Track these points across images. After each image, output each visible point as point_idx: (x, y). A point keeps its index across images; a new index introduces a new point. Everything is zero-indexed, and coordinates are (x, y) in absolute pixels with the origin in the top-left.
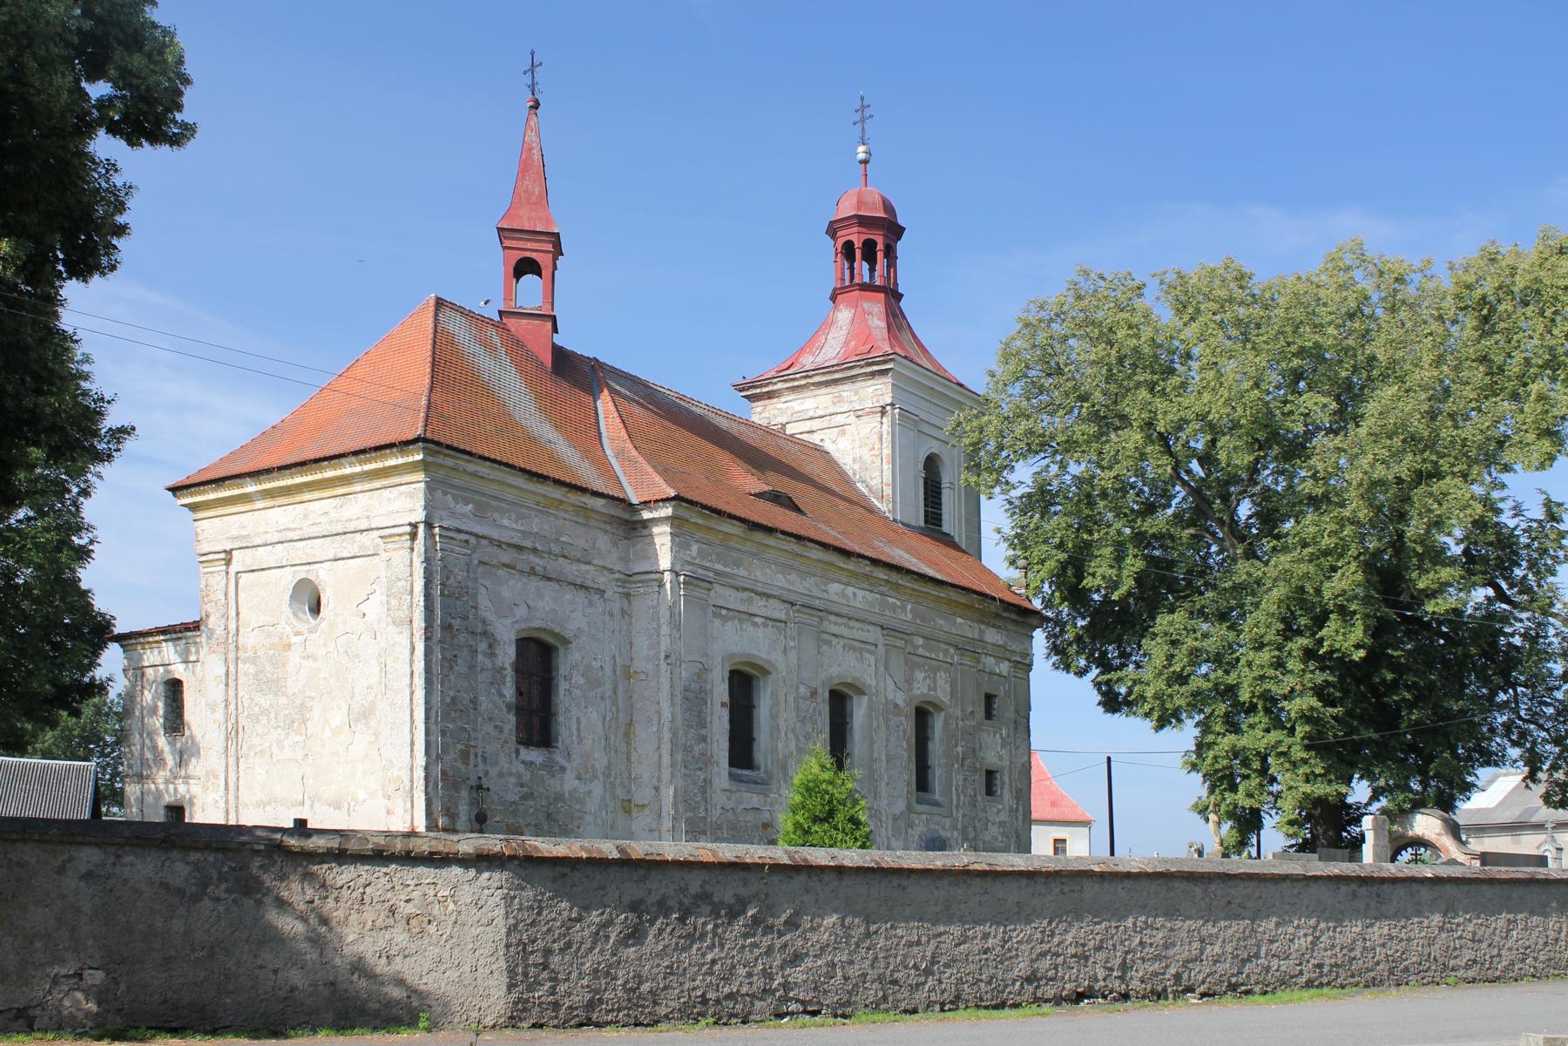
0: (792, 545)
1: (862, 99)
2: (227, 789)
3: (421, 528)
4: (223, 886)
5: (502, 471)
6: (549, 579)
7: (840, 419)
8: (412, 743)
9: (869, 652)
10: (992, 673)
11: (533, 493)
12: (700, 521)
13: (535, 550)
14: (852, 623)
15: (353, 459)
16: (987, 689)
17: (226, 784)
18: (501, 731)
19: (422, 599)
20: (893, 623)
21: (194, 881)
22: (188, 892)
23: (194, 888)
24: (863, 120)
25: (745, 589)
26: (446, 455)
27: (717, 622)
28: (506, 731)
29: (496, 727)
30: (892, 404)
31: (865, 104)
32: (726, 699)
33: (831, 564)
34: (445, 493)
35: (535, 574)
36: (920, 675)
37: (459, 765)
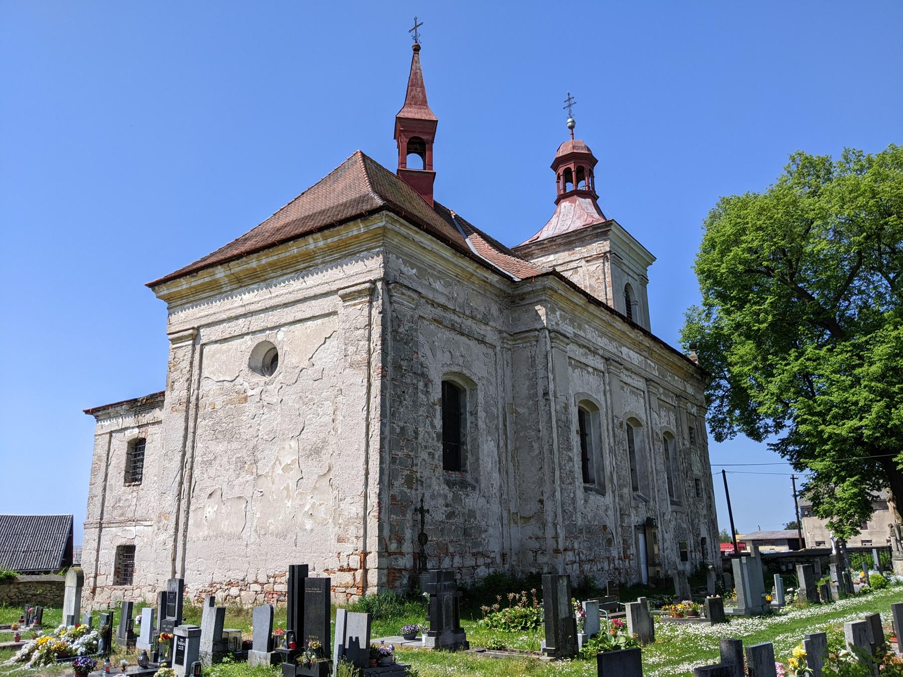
0: (607, 317)
1: (569, 94)
2: (177, 529)
3: (379, 285)
5: (438, 244)
6: (463, 334)
7: (574, 265)
12: (563, 293)
14: (633, 376)
15: (319, 235)
17: (177, 524)
19: (379, 343)
20: (651, 377)
25: (584, 347)
26: (402, 224)
27: (570, 369)
28: (437, 456)
29: (430, 454)
30: (610, 252)
31: (571, 96)
33: (624, 333)
34: (398, 258)
35: (455, 330)
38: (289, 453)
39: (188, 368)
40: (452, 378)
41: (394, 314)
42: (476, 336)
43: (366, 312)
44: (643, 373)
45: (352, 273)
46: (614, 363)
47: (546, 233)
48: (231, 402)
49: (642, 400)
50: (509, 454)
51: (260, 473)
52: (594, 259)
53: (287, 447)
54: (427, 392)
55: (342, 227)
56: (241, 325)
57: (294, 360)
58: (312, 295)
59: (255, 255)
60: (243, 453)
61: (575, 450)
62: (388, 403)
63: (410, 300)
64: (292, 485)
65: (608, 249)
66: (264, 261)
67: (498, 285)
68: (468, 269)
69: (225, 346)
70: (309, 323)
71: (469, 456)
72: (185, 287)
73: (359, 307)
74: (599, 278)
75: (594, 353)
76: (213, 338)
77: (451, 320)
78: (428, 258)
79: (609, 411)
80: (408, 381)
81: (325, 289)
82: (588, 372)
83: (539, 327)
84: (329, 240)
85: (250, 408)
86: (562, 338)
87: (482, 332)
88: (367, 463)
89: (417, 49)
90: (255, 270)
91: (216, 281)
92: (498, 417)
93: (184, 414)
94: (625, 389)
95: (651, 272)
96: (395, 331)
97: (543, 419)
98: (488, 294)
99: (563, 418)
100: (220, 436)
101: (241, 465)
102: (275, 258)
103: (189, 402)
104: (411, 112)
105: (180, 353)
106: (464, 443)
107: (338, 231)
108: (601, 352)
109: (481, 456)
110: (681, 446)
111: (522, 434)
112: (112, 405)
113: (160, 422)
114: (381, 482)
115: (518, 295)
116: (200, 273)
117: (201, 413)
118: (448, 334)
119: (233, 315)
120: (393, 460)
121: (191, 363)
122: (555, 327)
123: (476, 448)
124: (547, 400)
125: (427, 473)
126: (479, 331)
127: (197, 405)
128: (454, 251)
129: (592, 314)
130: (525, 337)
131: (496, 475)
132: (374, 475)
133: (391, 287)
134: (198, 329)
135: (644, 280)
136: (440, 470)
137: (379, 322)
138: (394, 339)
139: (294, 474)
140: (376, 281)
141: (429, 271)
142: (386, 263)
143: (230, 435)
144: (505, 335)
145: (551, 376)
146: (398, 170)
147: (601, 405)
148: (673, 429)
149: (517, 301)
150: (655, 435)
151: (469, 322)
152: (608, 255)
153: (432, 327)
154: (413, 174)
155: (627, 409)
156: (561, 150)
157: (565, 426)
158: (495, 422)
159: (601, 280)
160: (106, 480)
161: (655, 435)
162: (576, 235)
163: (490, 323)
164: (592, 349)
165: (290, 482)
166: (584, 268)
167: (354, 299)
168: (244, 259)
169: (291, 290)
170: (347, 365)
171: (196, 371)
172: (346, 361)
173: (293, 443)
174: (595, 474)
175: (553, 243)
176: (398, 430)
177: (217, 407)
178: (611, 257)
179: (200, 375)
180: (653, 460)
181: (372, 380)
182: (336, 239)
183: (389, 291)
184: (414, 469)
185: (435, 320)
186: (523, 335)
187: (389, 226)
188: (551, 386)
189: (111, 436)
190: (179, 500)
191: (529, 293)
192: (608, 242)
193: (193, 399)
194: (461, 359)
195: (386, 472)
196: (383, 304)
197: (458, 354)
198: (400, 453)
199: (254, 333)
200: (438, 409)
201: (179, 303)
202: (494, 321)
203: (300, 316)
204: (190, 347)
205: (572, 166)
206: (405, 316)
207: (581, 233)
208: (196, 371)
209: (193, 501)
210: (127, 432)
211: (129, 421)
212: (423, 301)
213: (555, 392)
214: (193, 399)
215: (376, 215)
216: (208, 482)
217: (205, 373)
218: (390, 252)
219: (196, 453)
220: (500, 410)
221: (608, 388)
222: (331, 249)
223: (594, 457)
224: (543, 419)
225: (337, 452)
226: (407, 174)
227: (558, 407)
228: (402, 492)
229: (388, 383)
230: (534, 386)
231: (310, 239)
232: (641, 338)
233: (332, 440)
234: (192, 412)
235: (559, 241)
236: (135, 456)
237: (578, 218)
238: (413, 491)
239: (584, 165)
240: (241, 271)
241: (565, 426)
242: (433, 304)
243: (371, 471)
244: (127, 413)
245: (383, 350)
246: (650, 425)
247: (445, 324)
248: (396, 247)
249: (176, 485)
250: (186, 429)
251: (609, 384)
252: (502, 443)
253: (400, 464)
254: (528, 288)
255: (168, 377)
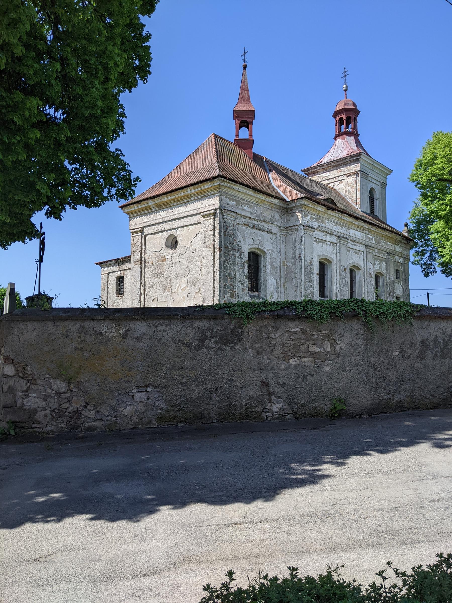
1: (345, 69)
3: (218, 211)
4: (214, 340)
5: (245, 189)
6: (259, 230)
7: (340, 178)
8: (214, 292)
9: (361, 254)
10: (398, 262)
11: (255, 197)
12: (311, 206)
13: (255, 219)
14: (357, 244)
15: (192, 187)
16: (396, 268)
18: (244, 286)
19: (218, 237)
20: (369, 244)
21: (197, 338)
22: (194, 345)
23: (197, 342)
24: (345, 76)
25: (325, 232)
26: (227, 182)
27: (315, 243)
28: (245, 285)
29: (242, 284)
30: (360, 170)
31: (346, 70)
32: (318, 272)
33: (351, 222)
34: (226, 197)
35: (255, 228)
36: (376, 263)
37: (230, 298)
38: (184, 283)
39: (140, 246)
40: (254, 250)
41: (225, 224)
42: (266, 230)
43: (212, 223)
44: (363, 242)
45: (206, 205)
46: (342, 239)
47: (326, 160)
48: (159, 261)
49: (362, 257)
50: (282, 284)
51: (172, 291)
52: (351, 175)
53: (183, 280)
54: (241, 257)
55: (202, 184)
56: (160, 227)
57: (184, 244)
58: (190, 214)
59: (166, 195)
60: (165, 283)
61: (315, 282)
62: (222, 263)
63: (232, 217)
64: (186, 296)
65: (359, 169)
66: (170, 198)
67: (278, 204)
68: (262, 198)
69: (155, 236)
70: (190, 227)
71: (262, 285)
72: (136, 208)
73: (210, 221)
74: (353, 186)
75: (331, 234)
76: (150, 232)
77: (253, 224)
78: (241, 196)
79: (338, 263)
80: (232, 253)
81: (195, 212)
82: (327, 244)
83: (298, 224)
84: (197, 190)
85: (167, 264)
86: (310, 229)
87: (269, 228)
88: (214, 287)
89: (245, 67)
90: (166, 202)
91: (149, 206)
92: (277, 268)
93: (140, 266)
94: (351, 252)
95: (390, 179)
96: (225, 231)
97: (298, 268)
98: (273, 209)
99: (309, 267)
100: (155, 276)
101: (165, 288)
102: (174, 197)
103: (141, 260)
104: (241, 106)
105: (136, 239)
106: (260, 280)
107: (200, 186)
108: (335, 233)
109: (267, 286)
110: (388, 279)
111: (288, 275)
112: (108, 261)
113: (130, 269)
114: (220, 295)
115: (289, 208)
116: (142, 202)
117: (147, 265)
118: (252, 230)
119: (158, 222)
120: (225, 287)
121: (141, 243)
122: (307, 224)
123: (265, 281)
124: (300, 259)
125: (240, 292)
126: (268, 227)
127: (145, 262)
128: (254, 191)
129: (330, 215)
130: (292, 229)
131: (275, 294)
132: (217, 292)
133: (223, 211)
134: (143, 228)
135: (384, 185)
136: (247, 291)
137: (218, 228)
138: (225, 235)
139: (186, 292)
140: (216, 209)
141: (242, 201)
142: (221, 201)
143: (159, 275)
144: (282, 228)
145: (303, 248)
146: (235, 140)
147: (334, 260)
148: (383, 271)
149: (289, 211)
150: (368, 274)
151: (263, 223)
152: (359, 172)
153: (244, 228)
154: (243, 141)
155: (351, 261)
156: (338, 106)
157: (309, 272)
158: (276, 270)
159: (354, 188)
160: (108, 294)
161: (368, 274)
162: (342, 161)
163: (274, 223)
164: (330, 232)
165: (184, 295)
166: (346, 180)
167: (208, 217)
168: (161, 197)
169: (181, 212)
170: (205, 247)
171: (143, 247)
172: (205, 244)
173: (185, 279)
174: (328, 294)
175: (329, 166)
176: (227, 274)
177: (154, 263)
178: (362, 174)
179: (145, 248)
180: (366, 287)
181: (215, 253)
182: (199, 189)
183: (222, 213)
184: (234, 290)
185: (245, 224)
186: (291, 228)
187: (222, 184)
188: (303, 253)
189: (108, 275)
190: (140, 302)
191: (294, 207)
192: (359, 165)
193: (143, 259)
194: (258, 242)
195: (222, 291)
196: (220, 219)
197: (257, 239)
198: (228, 284)
199: (167, 231)
200: (246, 265)
201: (134, 215)
202: (276, 222)
203: (186, 224)
204: (140, 236)
205: (344, 116)
206: (230, 224)
207: (344, 159)
208: (143, 247)
209: (146, 303)
210: (115, 273)
211: (116, 268)
212: (239, 216)
213: (305, 255)
214: (143, 259)
215: (216, 179)
216: (152, 295)
217: (147, 248)
218: (222, 195)
219: (146, 283)
220: (278, 264)
221: (338, 251)
222: (198, 194)
223: (328, 284)
224: (298, 268)
225: (202, 283)
226: (239, 141)
227: (306, 262)
228: (229, 299)
229: (222, 255)
230: (295, 253)
231: (188, 189)
232: (362, 224)
233: (200, 278)
234: (143, 265)
235: (332, 164)
236: (120, 284)
237: (345, 149)
238: (234, 299)
239: (351, 115)
240: (160, 202)
241: (309, 272)
242: (244, 217)
243: (216, 291)
244: (115, 265)
245: (220, 240)
246: (366, 269)
247: (250, 226)
248: (225, 193)
249: (139, 296)
250: (141, 272)
251: (340, 249)
252: (278, 280)
253: (228, 288)
254: (293, 205)
255: (131, 249)
